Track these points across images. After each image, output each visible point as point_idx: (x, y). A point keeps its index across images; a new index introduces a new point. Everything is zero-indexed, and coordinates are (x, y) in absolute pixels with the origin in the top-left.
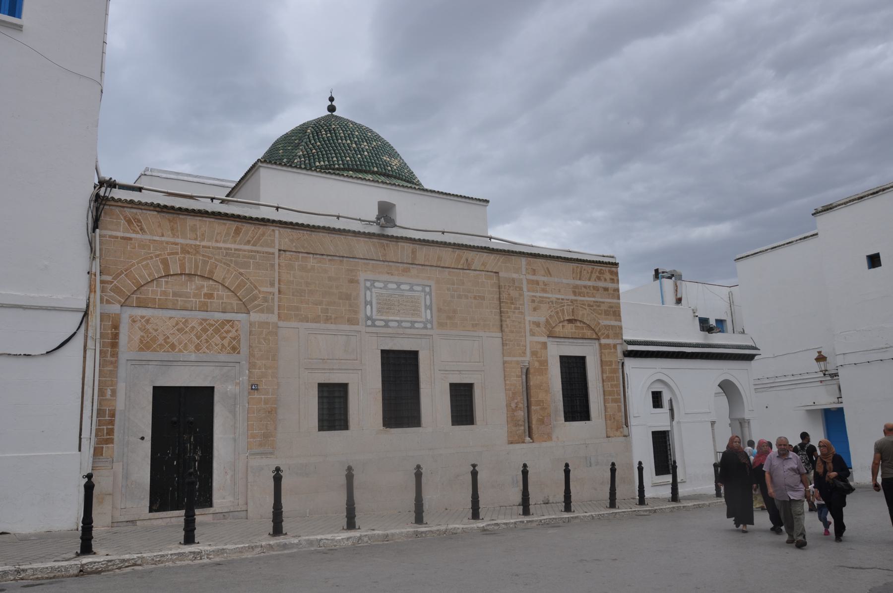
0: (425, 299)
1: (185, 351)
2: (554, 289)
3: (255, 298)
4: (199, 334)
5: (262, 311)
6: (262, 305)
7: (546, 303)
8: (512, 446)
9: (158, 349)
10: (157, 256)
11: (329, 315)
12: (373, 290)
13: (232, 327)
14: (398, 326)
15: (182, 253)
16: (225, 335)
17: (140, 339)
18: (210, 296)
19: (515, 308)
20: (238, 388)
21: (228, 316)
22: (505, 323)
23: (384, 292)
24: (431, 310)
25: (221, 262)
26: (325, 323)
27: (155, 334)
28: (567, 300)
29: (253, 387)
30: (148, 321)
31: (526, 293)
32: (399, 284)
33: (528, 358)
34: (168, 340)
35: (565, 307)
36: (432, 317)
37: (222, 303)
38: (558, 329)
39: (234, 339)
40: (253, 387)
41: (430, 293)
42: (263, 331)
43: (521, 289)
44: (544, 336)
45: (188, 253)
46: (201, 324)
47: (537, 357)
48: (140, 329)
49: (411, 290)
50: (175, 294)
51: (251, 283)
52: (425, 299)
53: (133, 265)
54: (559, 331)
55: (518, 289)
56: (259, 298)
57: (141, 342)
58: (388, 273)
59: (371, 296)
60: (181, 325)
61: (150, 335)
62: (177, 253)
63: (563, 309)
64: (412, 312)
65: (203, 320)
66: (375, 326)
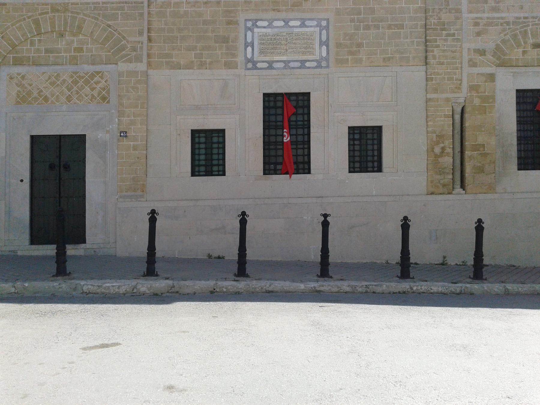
0: (320, 34)
1: (57, 103)
2: (513, 6)
3: (123, 48)
4: (70, 86)
5: (130, 61)
6: (130, 54)
7: (497, 25)
8: (431, 198)
9: (33, 102)
10: (29, 18)
11: (204, 60)
12: (256, 30)
13: (102, 77)
14: (285, 66)
15: (52, 12)
16: (95, 86)
17: (17, 94)
18: (80, 50)
19: (448, 35)
20: (108, 135)
21: (98, 68)
22: (431, 54)
23: (269, 30)
24: (328, 46)
25: (89, 17)
26: (199, 69)
27: (29, 88)
28: (533, 17)
29: (122, 135)
30: (23, 77)
31: (465, 15)
32: (286, 21)
33: (461, 96)
34: (42, 93)
35: (529, 28)
36: (328, 53)
37: (91, 55)
38: (517, 54)
39: (104, 89)
40: (122, 135)
41: (327, 28)
42: (131, 80)
43: (458, 11)
44: (491, 67)
45: (58, 11)
46: (72, 77)
47: (478, 92)
48: (17, 84)
49: (303, 25)
50: (47, 51)
51: (119, 34)
52: (320, 34)
53: (8, 28)
54: (517, 60)
55: (453, 11)
56: (127, 48)
57: (18, 96)
58: (274, 10)
59: (253, 36)
60: (53, 79)
61: (25, 90)
62: (47, 13)
63: (526, 31)
64: (303, 50)
65: (73, 73)
66: (257, 68)
